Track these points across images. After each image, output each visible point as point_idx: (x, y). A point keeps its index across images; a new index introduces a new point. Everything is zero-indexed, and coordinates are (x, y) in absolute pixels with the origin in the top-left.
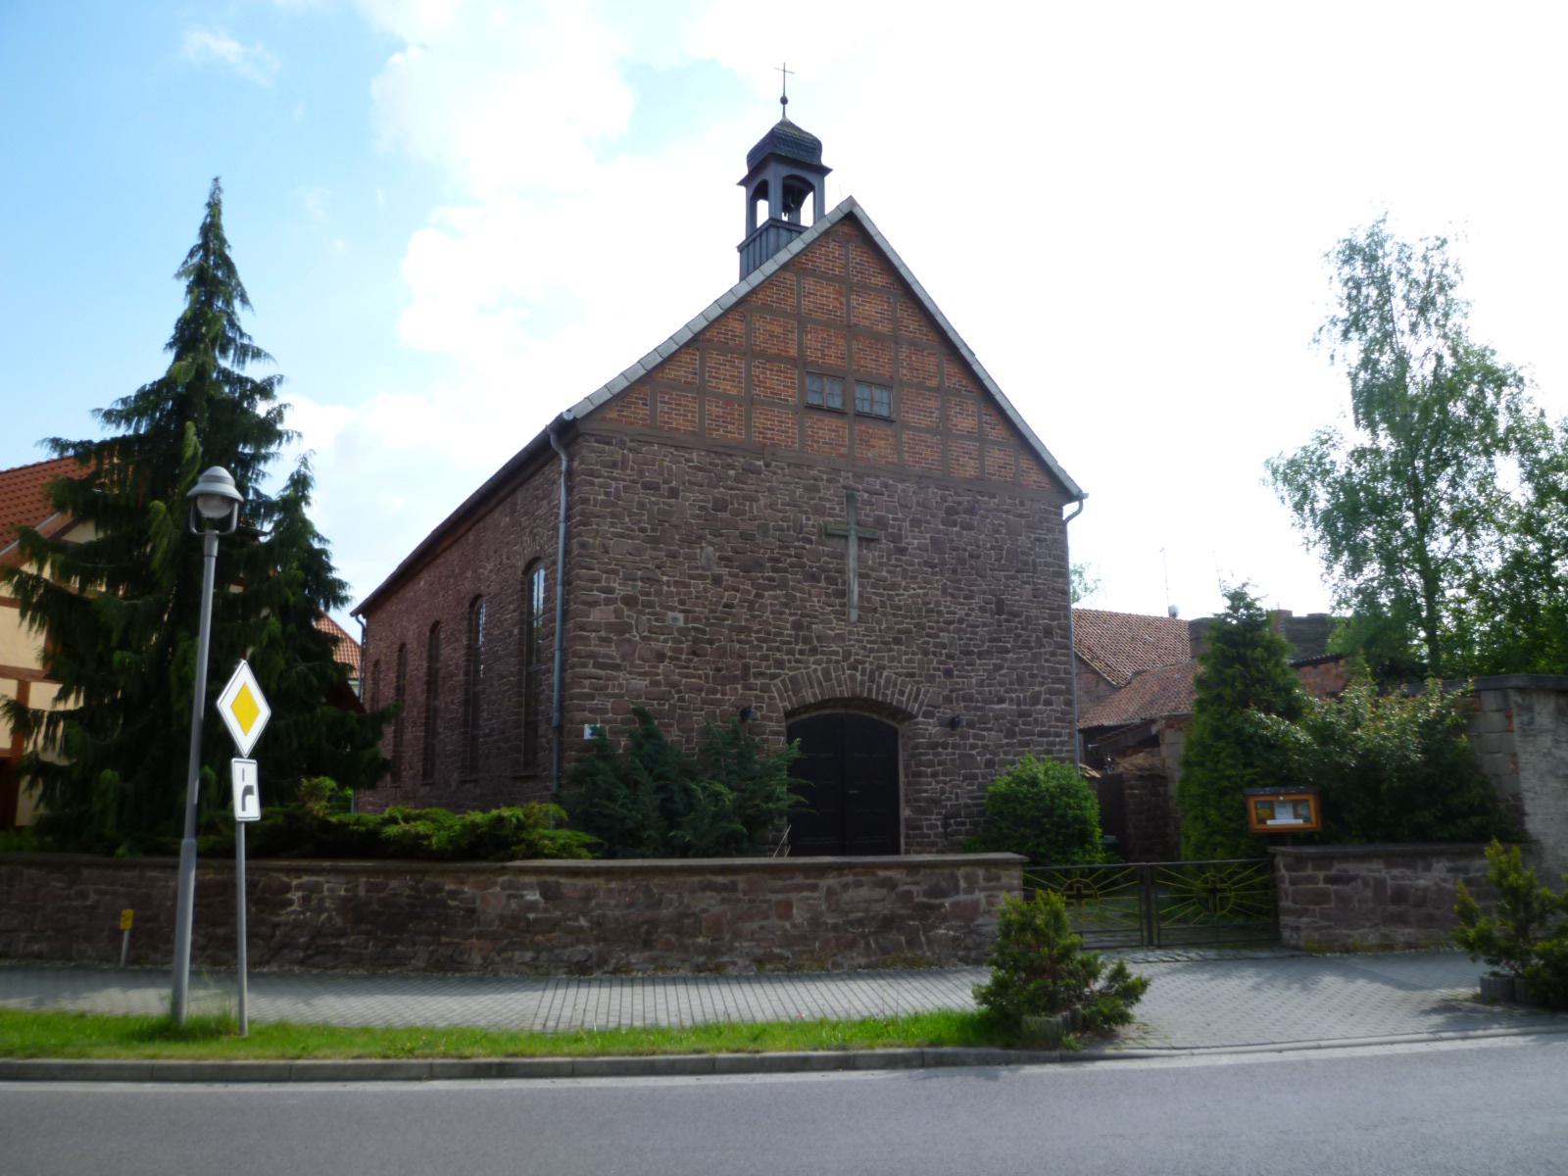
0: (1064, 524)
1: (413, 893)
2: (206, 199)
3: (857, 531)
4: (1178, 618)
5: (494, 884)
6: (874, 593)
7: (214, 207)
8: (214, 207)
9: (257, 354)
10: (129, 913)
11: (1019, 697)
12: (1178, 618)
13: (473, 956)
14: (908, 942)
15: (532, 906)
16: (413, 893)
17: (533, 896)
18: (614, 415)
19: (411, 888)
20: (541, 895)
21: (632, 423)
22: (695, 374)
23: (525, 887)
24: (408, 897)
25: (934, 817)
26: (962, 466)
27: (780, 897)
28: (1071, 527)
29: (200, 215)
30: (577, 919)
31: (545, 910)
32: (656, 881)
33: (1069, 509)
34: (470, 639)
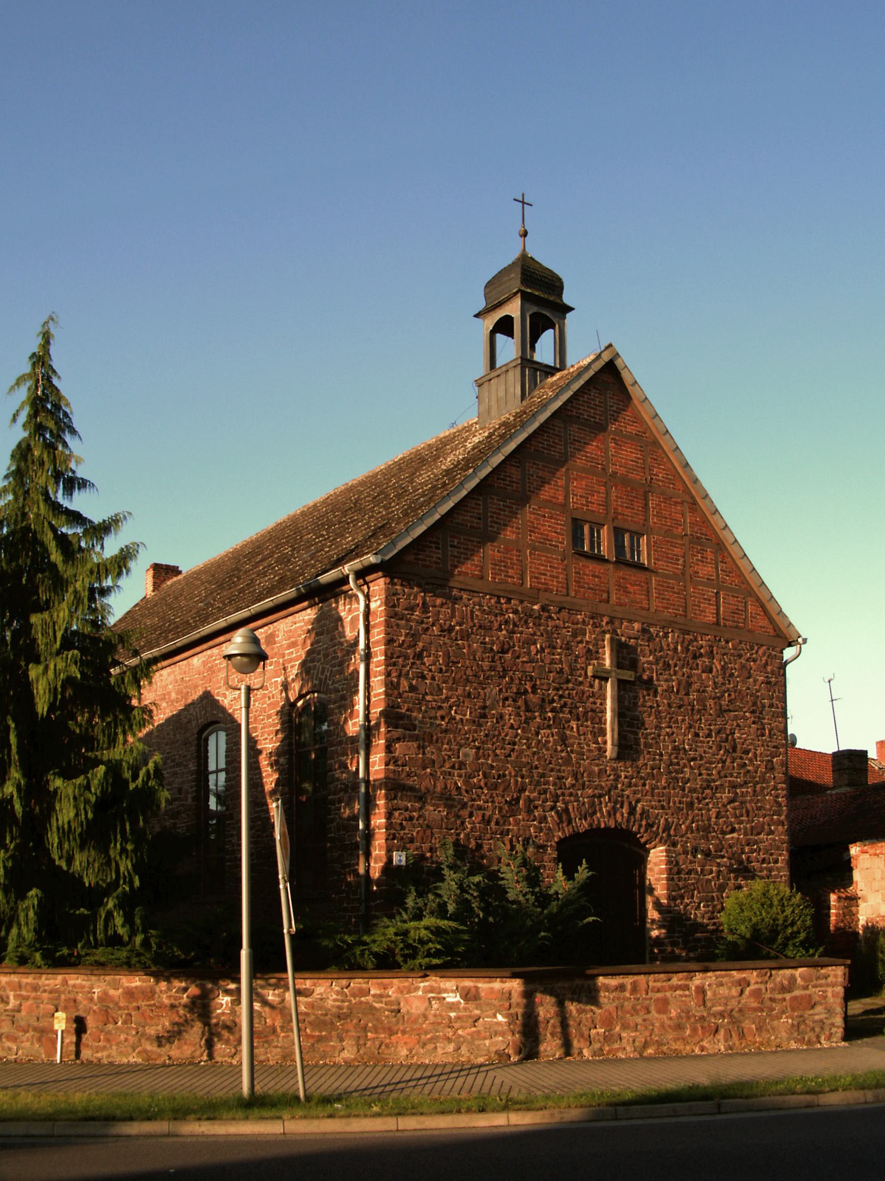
0: (783, 666)
1: (339, 997)
2: (39, 329)
3: (617, 674)
4: (797, 746)
5: (417, 989)
6: (630, 732)
7: (47, 338)
8: (47, 338)
9: (83, 484)
10: (61, 1015)
11: (745, 828)
12: (797, 746)
13: (400, 1048)
14: (757, 1029)
15: (453, 1007)
16: (339, 997)
17: (452, 998)
18: (411, 558)
19: (338, 993)
20: (461, 997)
21: (426, 566)
22: (480, 519)
23: (446, 991)
24: (335, 1000)
25: (676, 935)
26: (702, 611)
27: (659, 995)
28: (791, 671)
29: (34, 345)
30: (495, 1016)
31: (465, 1009)
32: (559, 984)
33: (788, 653)
34: (199, 765)
